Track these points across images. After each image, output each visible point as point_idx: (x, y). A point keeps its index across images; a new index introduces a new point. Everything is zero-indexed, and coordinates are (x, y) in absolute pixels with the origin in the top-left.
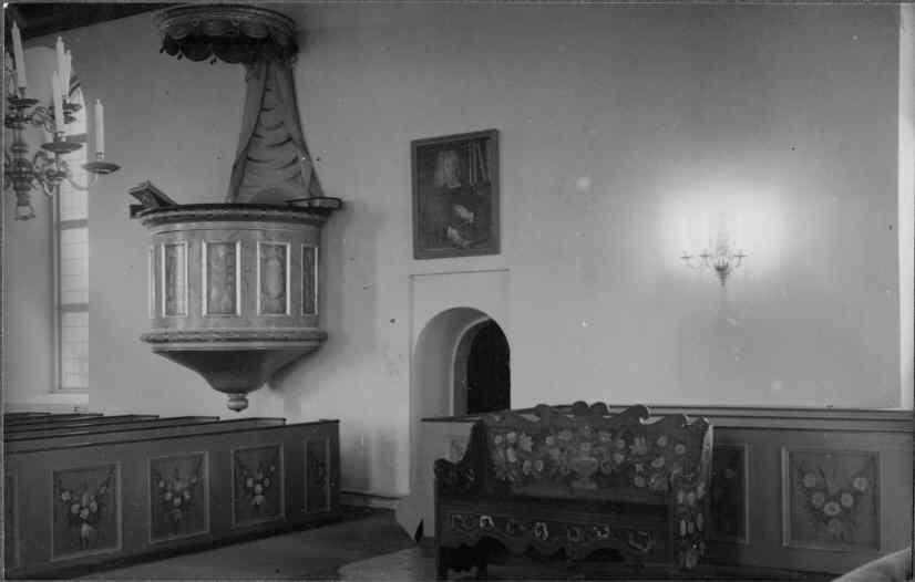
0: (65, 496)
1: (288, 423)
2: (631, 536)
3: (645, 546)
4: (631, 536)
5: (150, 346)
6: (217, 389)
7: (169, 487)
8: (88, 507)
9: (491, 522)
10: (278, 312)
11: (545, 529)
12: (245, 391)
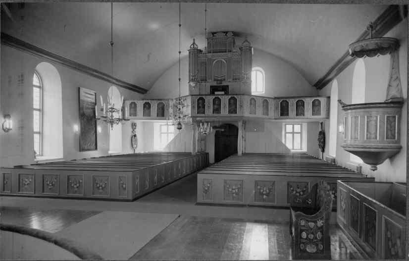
0: (259, 187)
1: (368, 177)
5: (342, 148)
6: (367, 163)
7: (295, 190)
8: (266, 191)
10: (391, 139)
12: (377, 164)
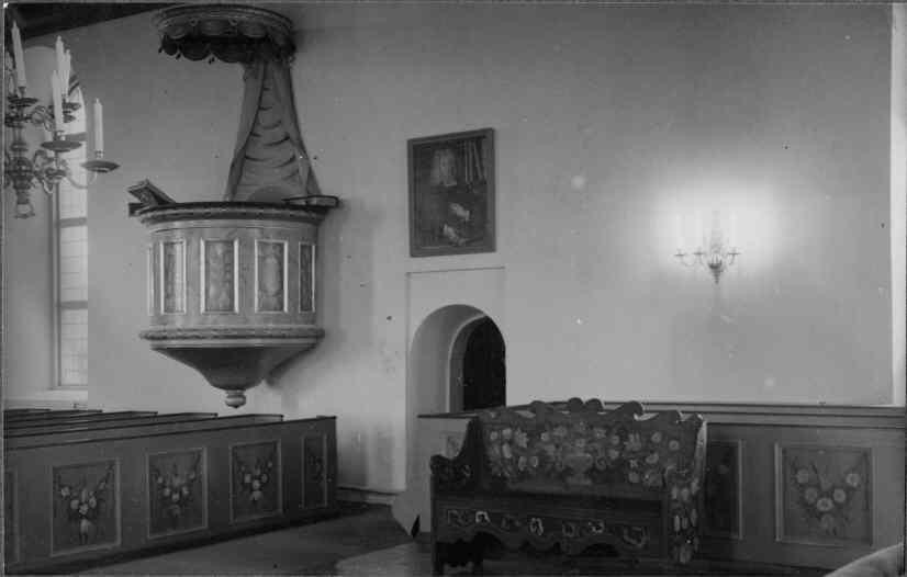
0: (65, 492)
1: (285, 419)
2: (626, 531)
3: (639, 541)
4: (626, 531)
5: (149, 343)
6: (216, 386)
7: (168, 483)
8: (87, 502)
9: (486, 518)
10: (275, 309)
11: (540, 525)
12: (243, 388)
